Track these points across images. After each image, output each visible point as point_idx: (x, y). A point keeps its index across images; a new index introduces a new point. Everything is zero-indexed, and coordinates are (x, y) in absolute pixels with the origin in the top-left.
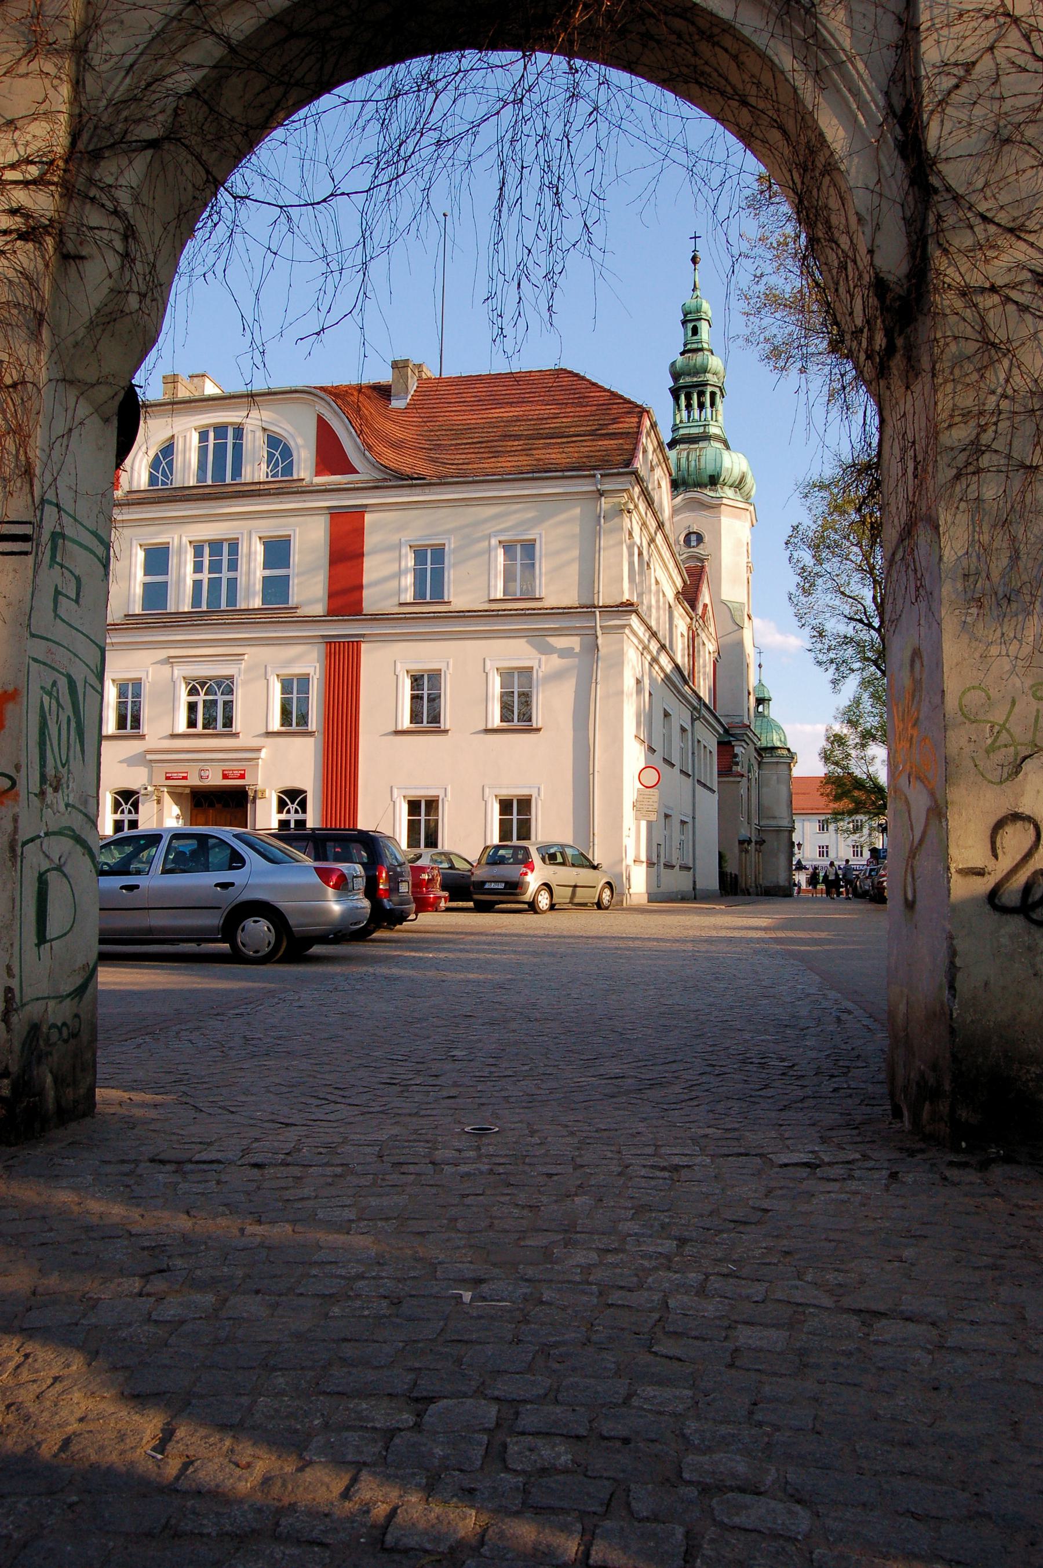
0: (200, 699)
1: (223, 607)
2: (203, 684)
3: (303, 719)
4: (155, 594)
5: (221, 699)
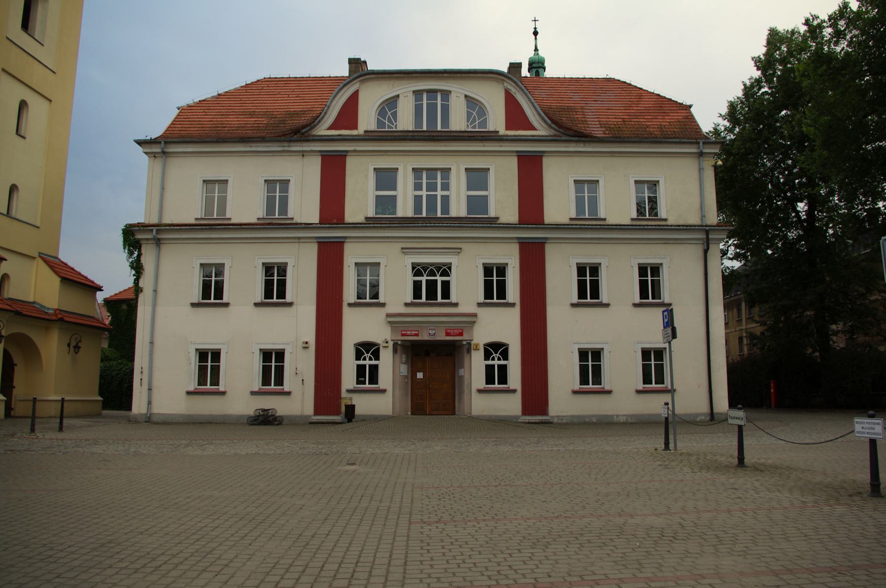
0: (424, 279)
1: (439, 215)
2: (438, 268)
3: (502, 294)
4: (386, 203)
5: (439, 279)
